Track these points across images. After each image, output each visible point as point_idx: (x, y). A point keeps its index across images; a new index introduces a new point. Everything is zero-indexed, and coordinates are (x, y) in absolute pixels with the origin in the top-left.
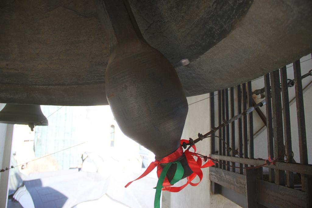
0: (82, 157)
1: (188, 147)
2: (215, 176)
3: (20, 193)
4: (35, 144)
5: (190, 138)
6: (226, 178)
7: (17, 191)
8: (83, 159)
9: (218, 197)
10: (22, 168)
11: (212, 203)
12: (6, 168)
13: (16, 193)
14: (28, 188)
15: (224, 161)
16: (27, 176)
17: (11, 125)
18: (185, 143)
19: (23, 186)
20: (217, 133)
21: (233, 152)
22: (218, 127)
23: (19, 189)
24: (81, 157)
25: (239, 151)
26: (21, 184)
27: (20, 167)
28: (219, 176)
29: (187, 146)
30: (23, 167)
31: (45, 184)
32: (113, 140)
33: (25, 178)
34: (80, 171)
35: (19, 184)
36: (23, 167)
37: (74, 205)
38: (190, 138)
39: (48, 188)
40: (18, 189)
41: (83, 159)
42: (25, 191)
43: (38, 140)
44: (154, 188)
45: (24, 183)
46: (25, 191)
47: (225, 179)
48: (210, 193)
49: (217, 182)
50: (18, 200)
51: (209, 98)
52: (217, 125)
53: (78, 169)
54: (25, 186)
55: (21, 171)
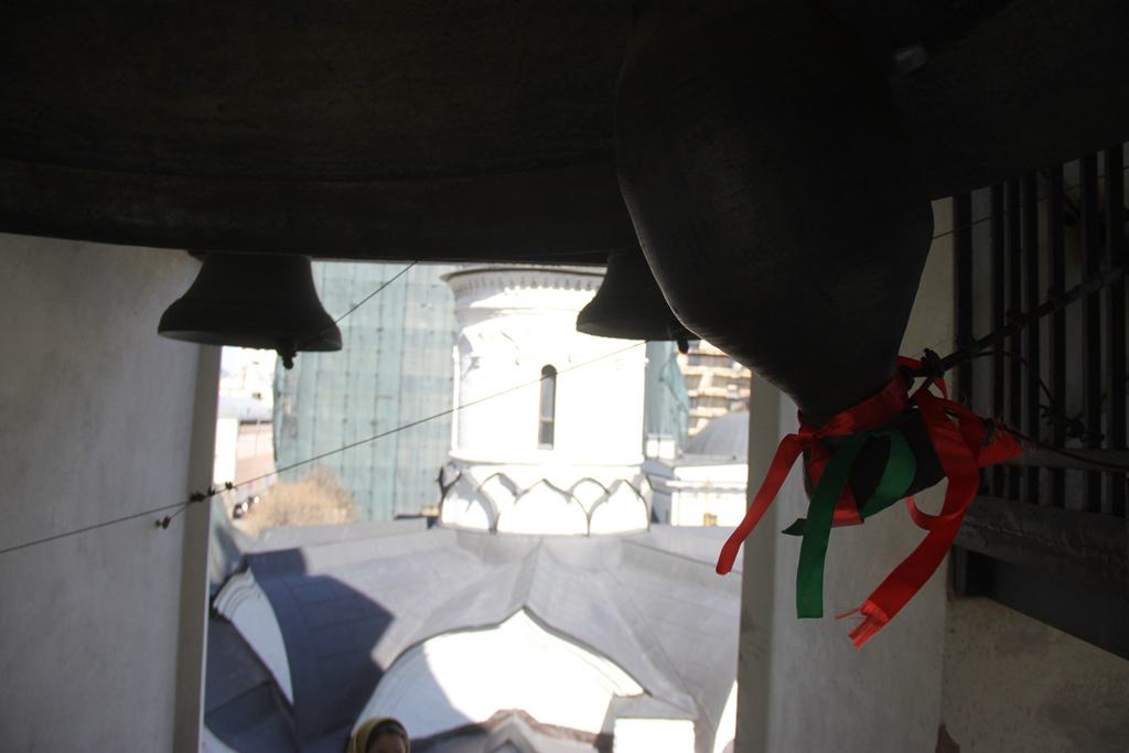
0: (441, 480)
1: (920, 385)
2: (975, 526)
3: (236, 591)
4: (278, 435)
5: (926, 350)
6: (1022, 532)
7: (227, 586)
8: (446, 484)
9: (979, 608)
10: (236, 516)
11: (953, 631)
12: (207, 489)
13: (220, 595)
14: (259, 579)
15: (1016, 470)
16: (253, 533)
17: (211, 348)
18: (908, 369)
19: (243, 569)
20: (983, 367)
21: (949, 488)
22: (987, 338)
23: (232, 579)
24: (437, 476)
25: (1084, 421)
26: (235, 565)
27: (230, 512)
28: (991, 528)
29: (916, 379)
30: (239, 511)
31: (319, 564)
32: (549, 419)
33: (245, 547)
34: (434, 528)
35: (228, 566)
36: (239, 511)
37: (415, 641)
38: (926, 350)
39: (329, 585)
40: (227, 579)
41: (446, 484)
42: (252, 587)
43: (286, 419)
44: (783, 532)
45: (247, 563)
46: (252, 587)
47: (1020, 534)
48: (948, 593)
49: (979, 546)
50: (228, 615)
51: (951, 236)
52: (983, 326)
53: (424, 522)
54: (249, 570)
55: (237, 524)
